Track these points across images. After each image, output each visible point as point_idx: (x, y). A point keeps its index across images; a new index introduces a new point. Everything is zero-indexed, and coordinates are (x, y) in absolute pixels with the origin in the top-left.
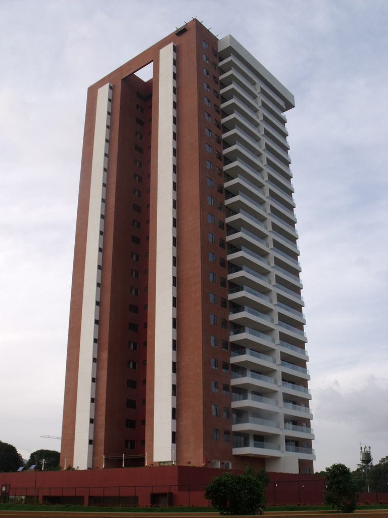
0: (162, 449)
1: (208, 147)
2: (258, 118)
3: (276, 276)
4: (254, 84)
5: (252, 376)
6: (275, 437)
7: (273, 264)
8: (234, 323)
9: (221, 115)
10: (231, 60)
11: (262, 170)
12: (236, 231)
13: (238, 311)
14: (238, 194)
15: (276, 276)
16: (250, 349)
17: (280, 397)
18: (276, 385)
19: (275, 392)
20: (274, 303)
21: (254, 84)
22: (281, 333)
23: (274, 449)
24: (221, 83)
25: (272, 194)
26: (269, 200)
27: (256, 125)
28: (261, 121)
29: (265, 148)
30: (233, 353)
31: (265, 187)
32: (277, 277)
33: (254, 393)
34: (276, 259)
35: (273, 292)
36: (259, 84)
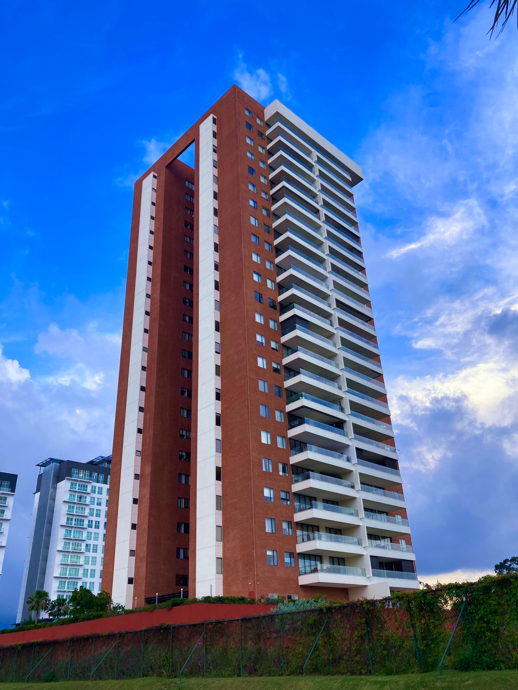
0: (207, 581)
1: (254, 219)
2: (325, 269)
3: (347, 379)
4: (309, 153)
5: (326, 509)
6: (357, 558)
7: (339, 345)
8: (302, 524)
9: (273, 236)
10: (280, 140)
11: (324, 260)
12: (302, 422)
13: (301, 451)
14: (291, 287)
15: (347, 379)
16: (321, 473)
17: (368, 562)
18: (364, 577)
19: (359, 557)
20: (344, 390)
21: (309, 153)
22: (354, 425)
23: (357, 575)
24: (275, 230)
25: (337, 285)
26: (319, 179)
27: (314, 196)
28: (325, 238)
29: (328, 253)
30: (293, 452)
31: (328, 279)
32: (349, 381)
33: (326, 501)
34: (342, 339)
35: (341, 377)
36: (316, 153)
